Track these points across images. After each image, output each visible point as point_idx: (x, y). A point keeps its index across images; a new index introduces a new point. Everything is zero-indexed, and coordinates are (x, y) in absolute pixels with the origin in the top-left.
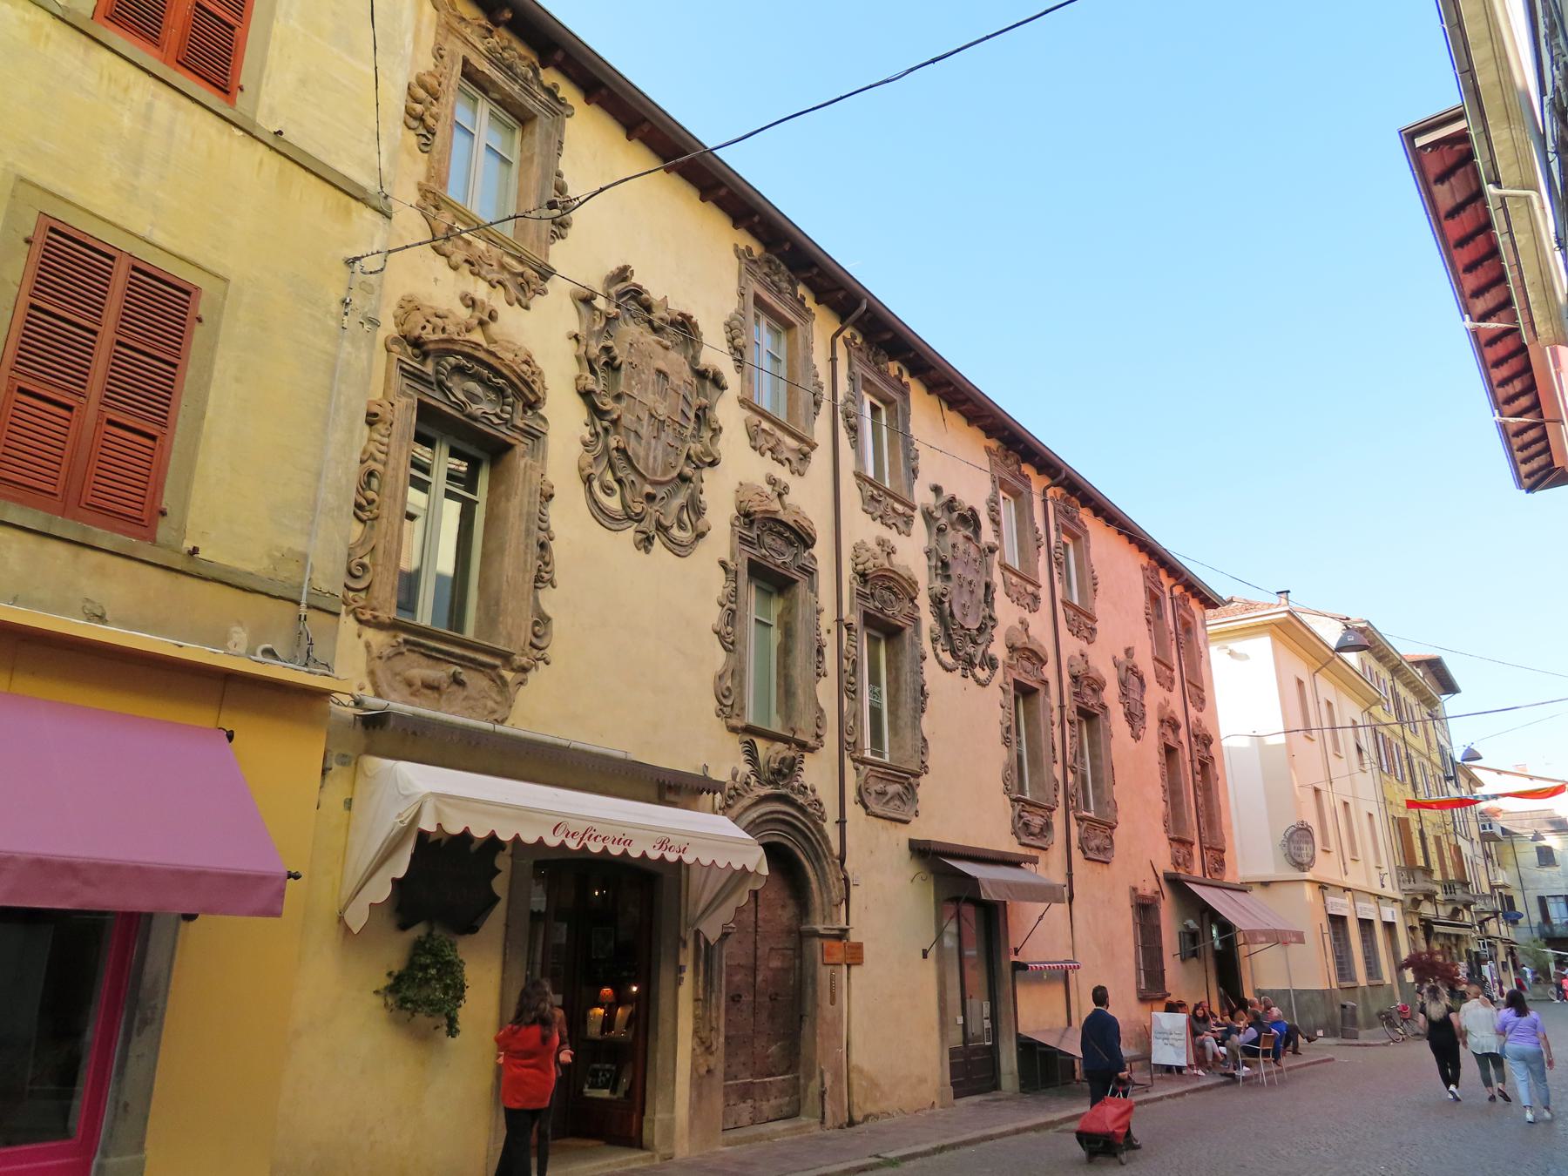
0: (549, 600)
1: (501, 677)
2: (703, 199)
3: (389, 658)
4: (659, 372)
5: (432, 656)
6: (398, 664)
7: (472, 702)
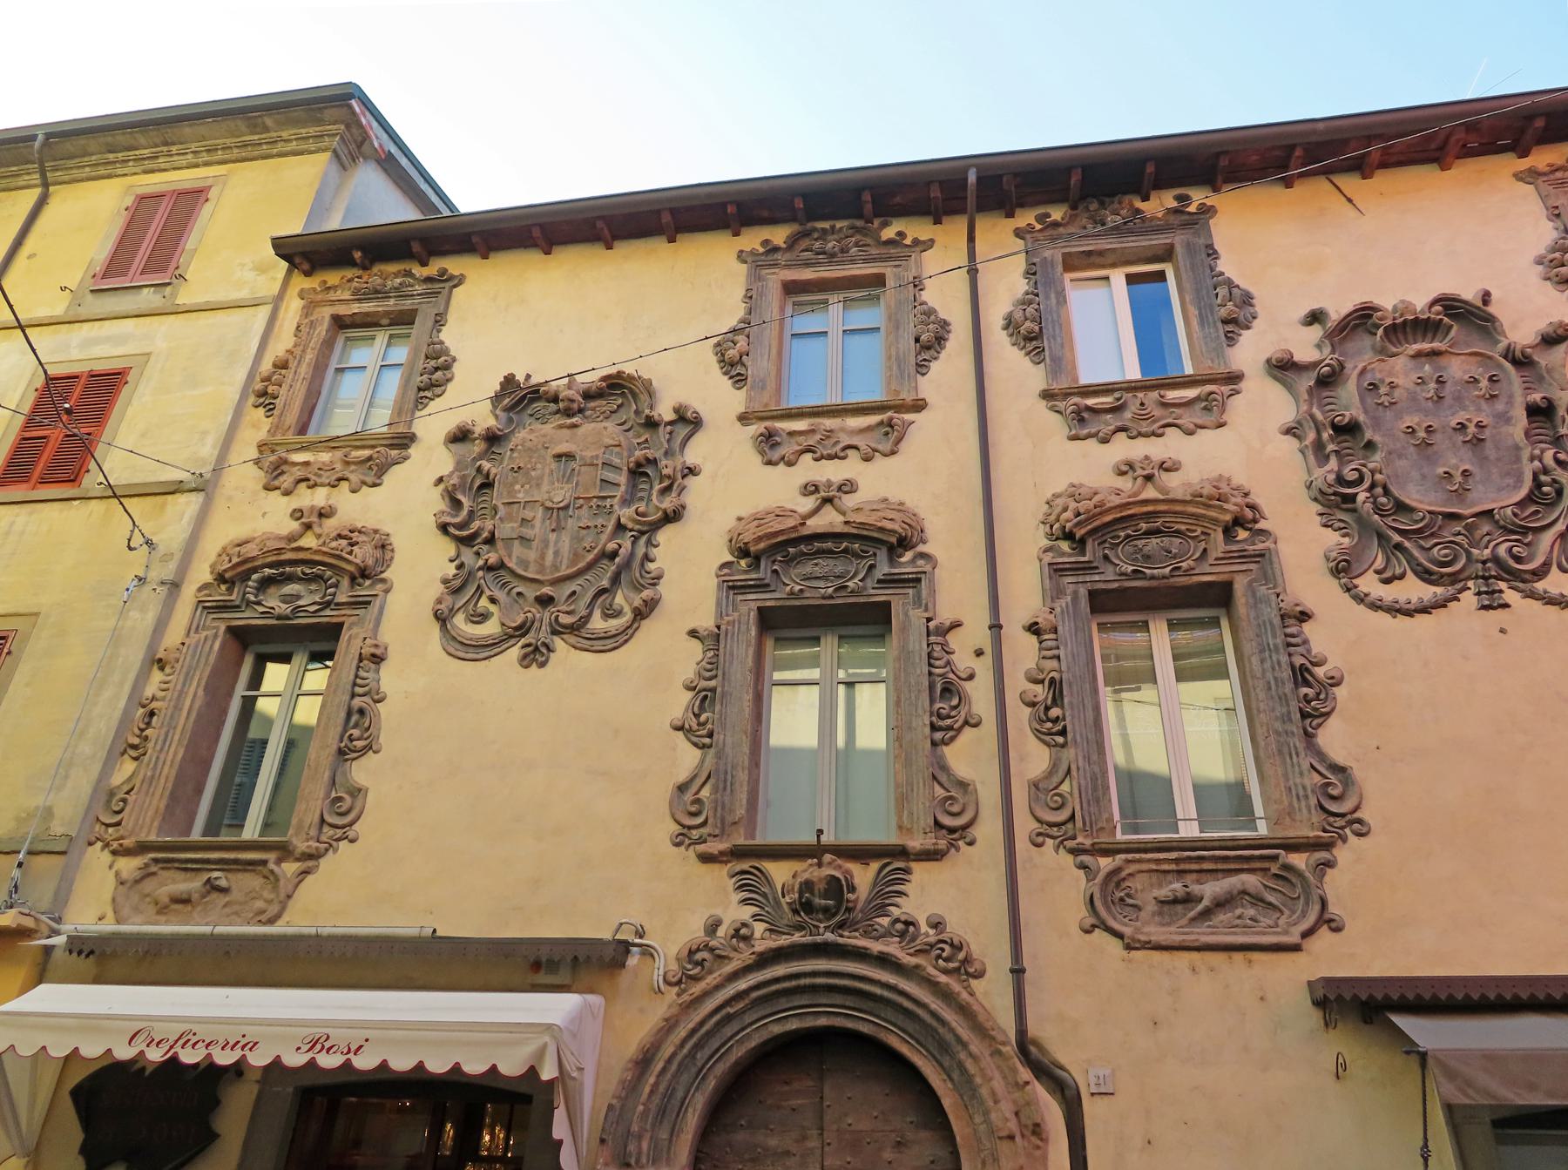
0: (361, 772)
1: (1287, 867)
2: (672, 240)
3: (137, 881)
4: (558, 456)
5: (186, 868)
6: (149, 886)
7: (236, 908)
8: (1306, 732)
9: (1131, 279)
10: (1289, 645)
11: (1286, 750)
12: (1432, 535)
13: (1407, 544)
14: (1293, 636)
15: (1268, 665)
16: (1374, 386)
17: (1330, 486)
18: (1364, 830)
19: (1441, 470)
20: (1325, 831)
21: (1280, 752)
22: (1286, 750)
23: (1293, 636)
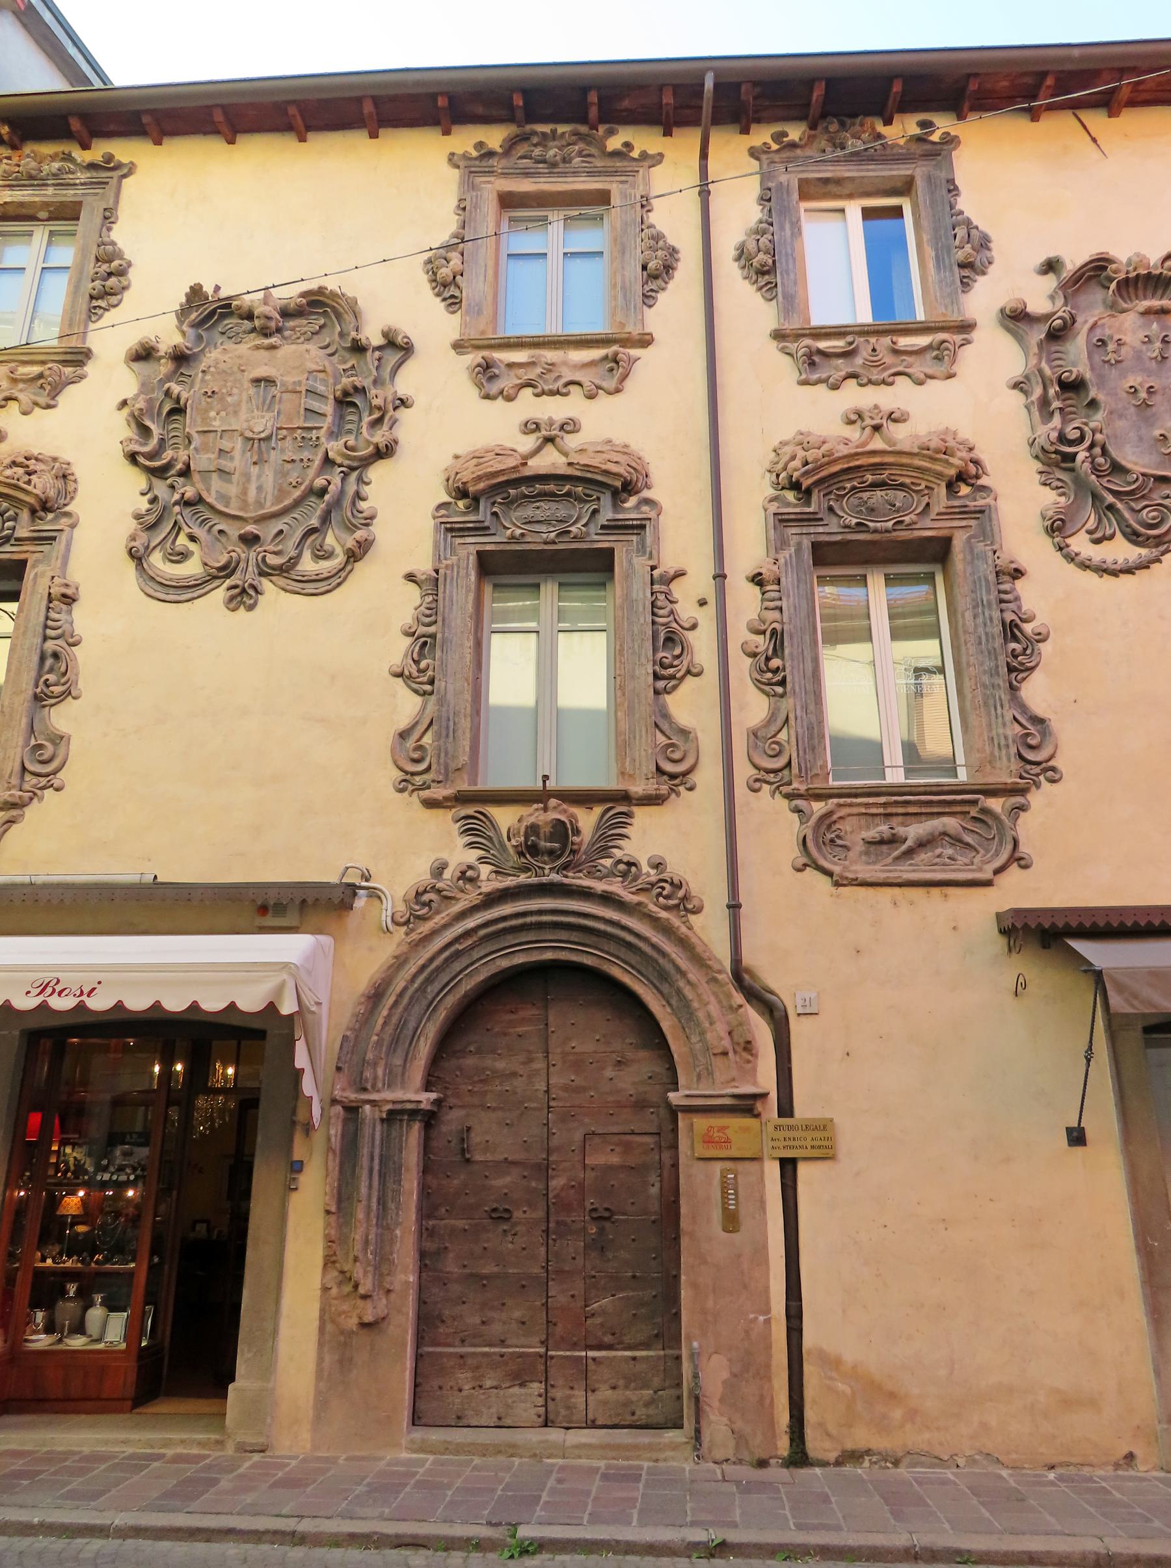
1: (985, 811)
4: (257, 381)
8: (1011, 687)
9: (869, 214)
10: (1002, 601)
11: (991, 702)
12: (1143, 497)
13: (1119, 505)
14: (1006, 592)
15: (980, 620)
16: (1103, 342)
17: (1052, 443)
18: (1057, 777)
19: (1157, 433)
20: (1021, 777)
21: (986, 704)
22: (991, 702)
23: (1006, 592)
